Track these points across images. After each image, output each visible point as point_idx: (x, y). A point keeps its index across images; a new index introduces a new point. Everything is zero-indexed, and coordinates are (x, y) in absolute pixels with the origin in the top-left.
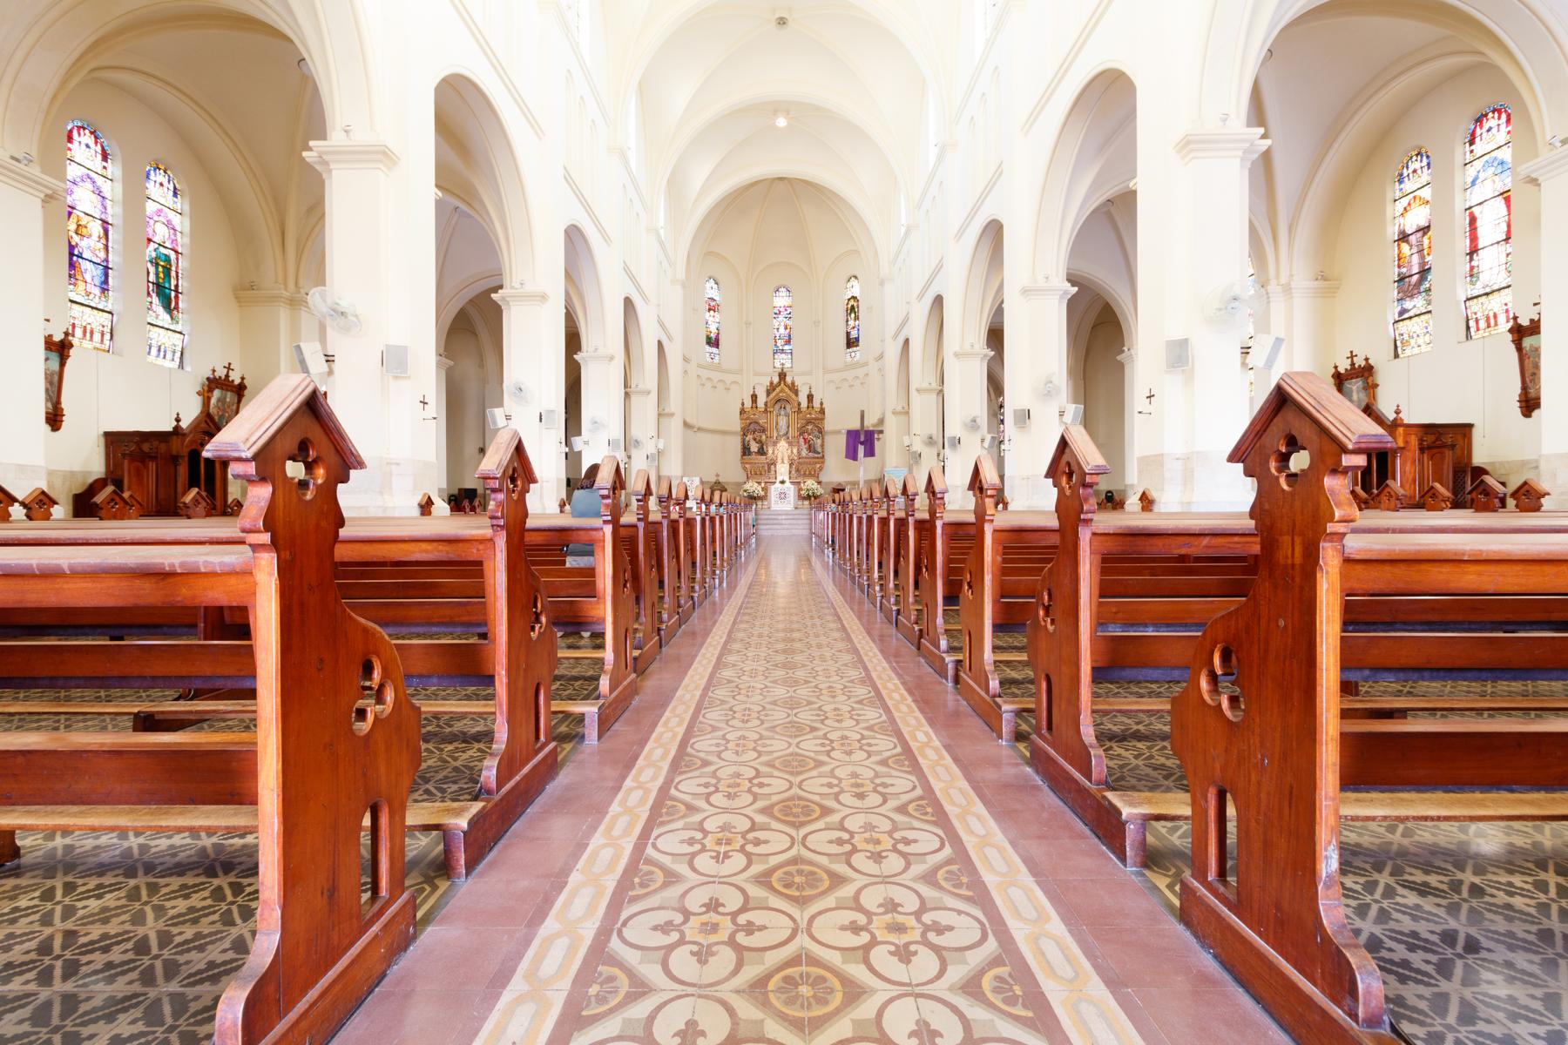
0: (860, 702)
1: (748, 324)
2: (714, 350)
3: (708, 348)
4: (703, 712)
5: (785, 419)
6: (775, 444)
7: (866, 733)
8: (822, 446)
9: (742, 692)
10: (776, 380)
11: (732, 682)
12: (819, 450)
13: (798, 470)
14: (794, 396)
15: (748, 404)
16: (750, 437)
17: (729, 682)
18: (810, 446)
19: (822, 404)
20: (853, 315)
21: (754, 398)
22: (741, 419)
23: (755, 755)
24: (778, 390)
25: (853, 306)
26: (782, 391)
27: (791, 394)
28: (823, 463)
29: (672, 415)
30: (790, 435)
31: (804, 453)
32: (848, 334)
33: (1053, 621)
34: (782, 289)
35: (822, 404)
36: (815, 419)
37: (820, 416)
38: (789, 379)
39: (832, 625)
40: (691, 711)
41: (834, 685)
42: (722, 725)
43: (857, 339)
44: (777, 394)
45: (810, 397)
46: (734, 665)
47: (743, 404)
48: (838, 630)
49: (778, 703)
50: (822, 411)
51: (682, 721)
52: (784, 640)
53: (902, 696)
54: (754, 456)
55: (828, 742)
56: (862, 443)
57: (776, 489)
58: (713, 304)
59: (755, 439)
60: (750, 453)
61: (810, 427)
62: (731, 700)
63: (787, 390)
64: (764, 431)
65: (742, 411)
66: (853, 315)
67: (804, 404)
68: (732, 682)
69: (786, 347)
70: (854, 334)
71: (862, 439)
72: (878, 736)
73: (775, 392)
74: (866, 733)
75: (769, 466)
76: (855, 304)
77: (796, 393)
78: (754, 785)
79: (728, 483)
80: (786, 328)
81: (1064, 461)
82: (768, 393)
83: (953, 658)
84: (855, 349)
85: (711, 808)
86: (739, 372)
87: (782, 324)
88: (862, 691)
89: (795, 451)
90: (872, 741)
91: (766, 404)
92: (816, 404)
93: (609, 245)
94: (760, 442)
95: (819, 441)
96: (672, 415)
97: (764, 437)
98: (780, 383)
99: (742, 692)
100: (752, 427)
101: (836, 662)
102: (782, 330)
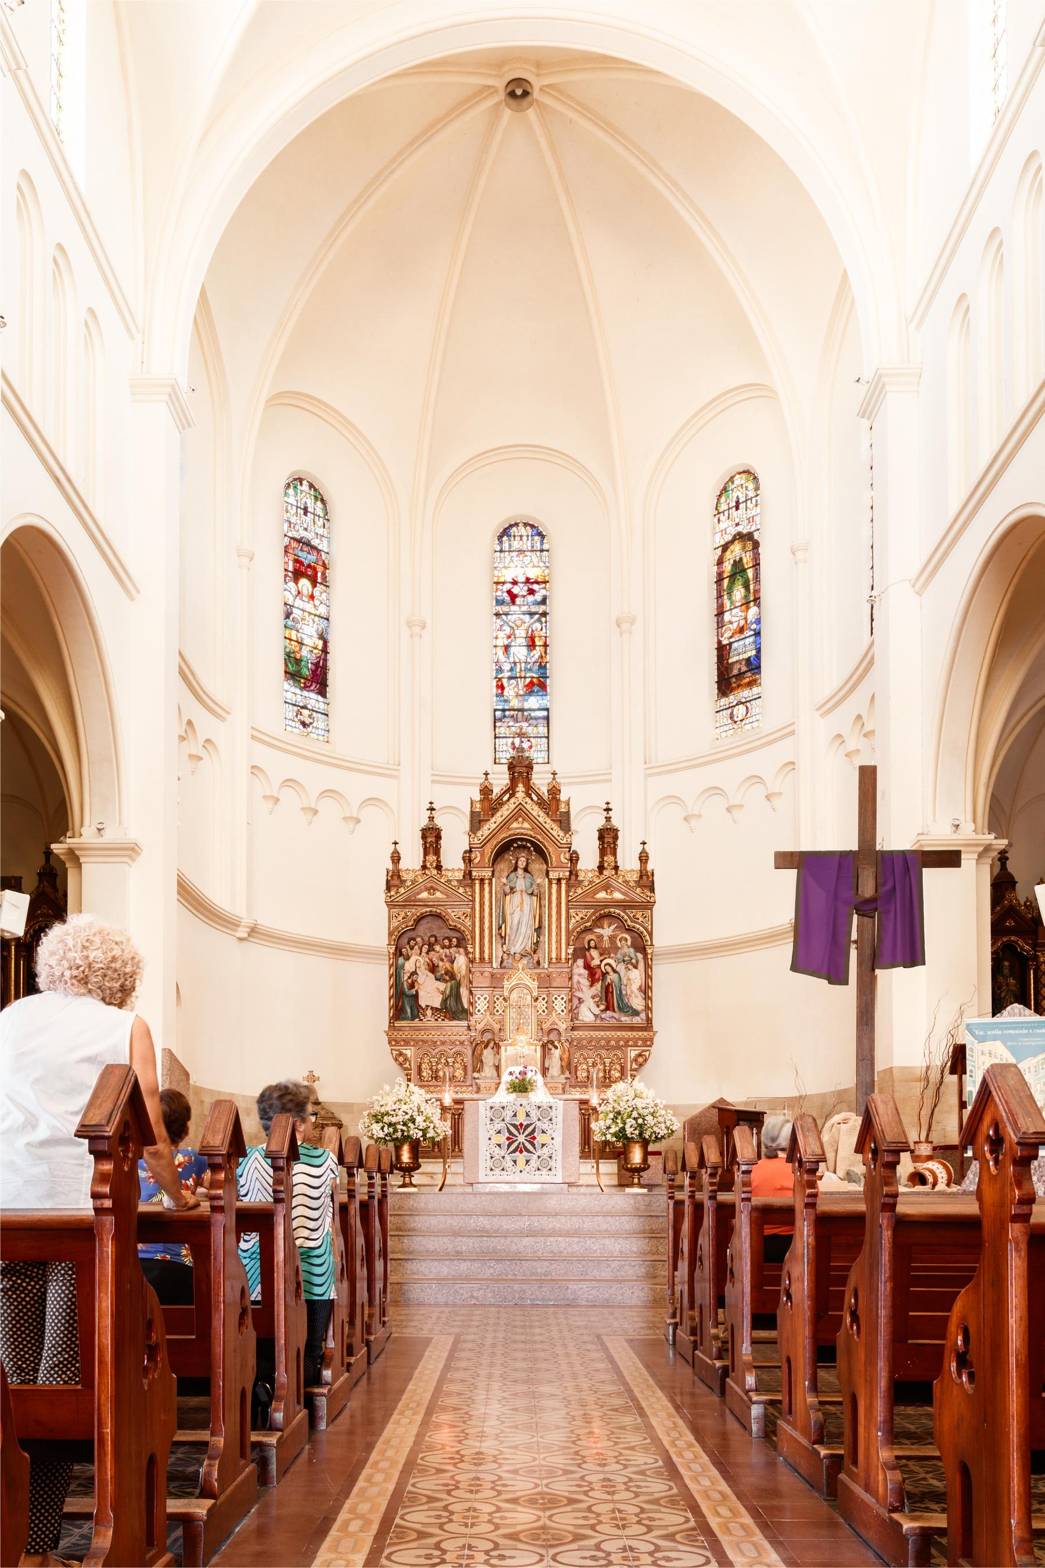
0: (671, 1537)
1: (417, 626)
2: (312, 699)
3: (293, 692)
4: (387, 1551)
5: (529, 904)
6: (496, 982)
7: (661, 1543)
8: (646, 990)
9: (454, 1517)
10: (500, 780)
11: (438, 1500)
12: (637, 1002)
13: (568, 1067)
14: (556, 831)
15: (412, 859)
16: (415, 961)
17: (422, 1535)
18: (607, 990)
19: (644, 858)
20: (739, 593)
21: (431, 838)
22: (391, 905)
23: (492, 1527)
24: (505, 811)
25: (738, 564)
26: (520, 813)
27: (549, 824)
28: (648, 1042)
29: (130, 851)
30: (543, 955)
31: (588, 1012)
32: (723, 651)
33: (971, 1377)
34: (522, 530)
35: (644, 858)
36: (624, 906)
37: (638, 895)
38: (540, 780)
39: (594, 1355)
40: (375, 1528)
41: (612, 1477)
42: (436, 1530)
43: (754, 665)
44: (505, 824)
45: (608, 838)
46: (431, 1499)
47: (396, 858)
48: (637, 1429)
49: (522, 1537)
50: (646, 880)
51: (368, 1523)
52: (532, 1502)
53: (703, 1466)
54: (429, 1019)
55: (603, 1555)
56: (865, 908)
57: (496, 1112)
58: (308, 558)
59: (433, 968)
60: (417, 1011)
61: (607, 931)
62: (437, 1531)
63: (536, 811)
64: (461, 943)
65: (394, 879)
66: (739, 593)
67: (589, 861)
68: (438, 1500)
69: (533, 702)
70: (742, 651)
71: (868, 888)
72: (663, 1509)
73: (498, 818)
74: (661, 1543)
75: (477, 1048)
76: (747, 560)
77: (564, 822)
78: (492, 1557)
79: (348, 1107)
80: (531, 645)
81: (987, 1120)
82: (476, 822)
83: (827, 1452)
84: (745, 694)
85: (446, 1534)
86: (388, 771)
87: (521, 633)
88: (675, 1519)
89: (560, 1005)
90: (673, 1555)
91: (468, 859)
92: (627, 859)
93: (132, 599)
94: (451, 975)
95: (636, 977)
96: (130, 851)
97: (461, 962)
98: (511, 790)
99: (454, 1517)
100: (423, 928)
101: (625, 1467)
102: (519, 652)
